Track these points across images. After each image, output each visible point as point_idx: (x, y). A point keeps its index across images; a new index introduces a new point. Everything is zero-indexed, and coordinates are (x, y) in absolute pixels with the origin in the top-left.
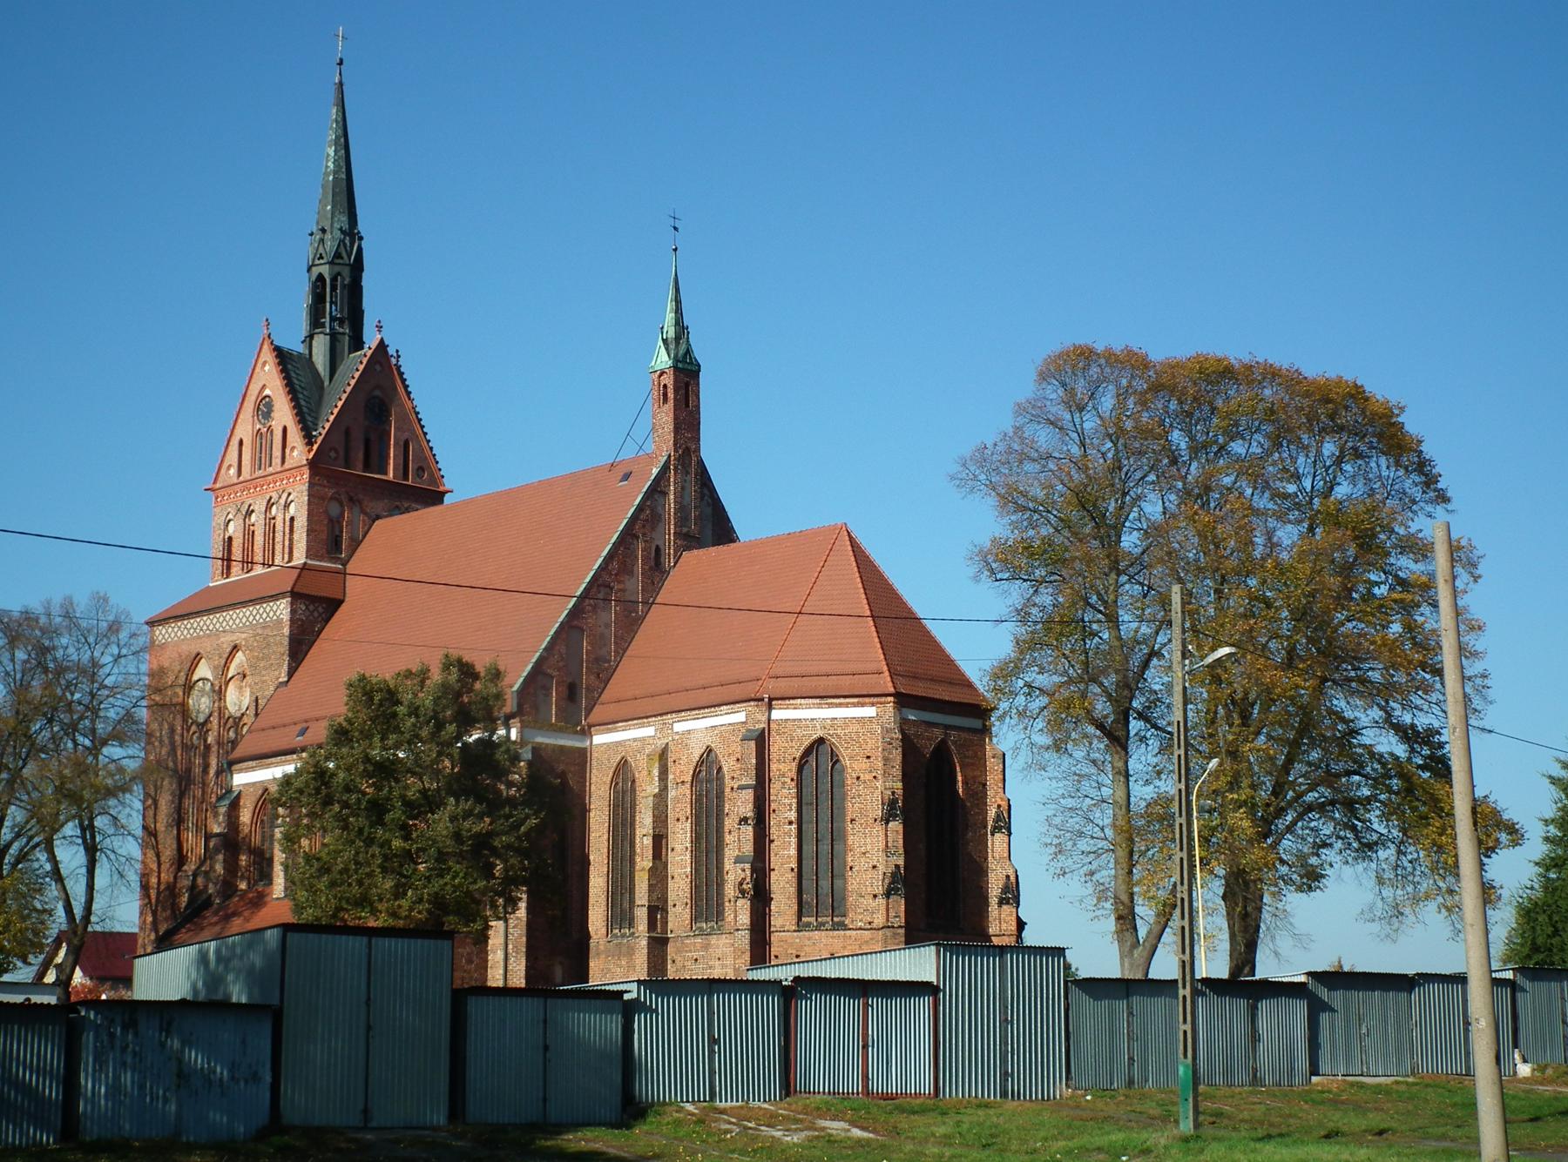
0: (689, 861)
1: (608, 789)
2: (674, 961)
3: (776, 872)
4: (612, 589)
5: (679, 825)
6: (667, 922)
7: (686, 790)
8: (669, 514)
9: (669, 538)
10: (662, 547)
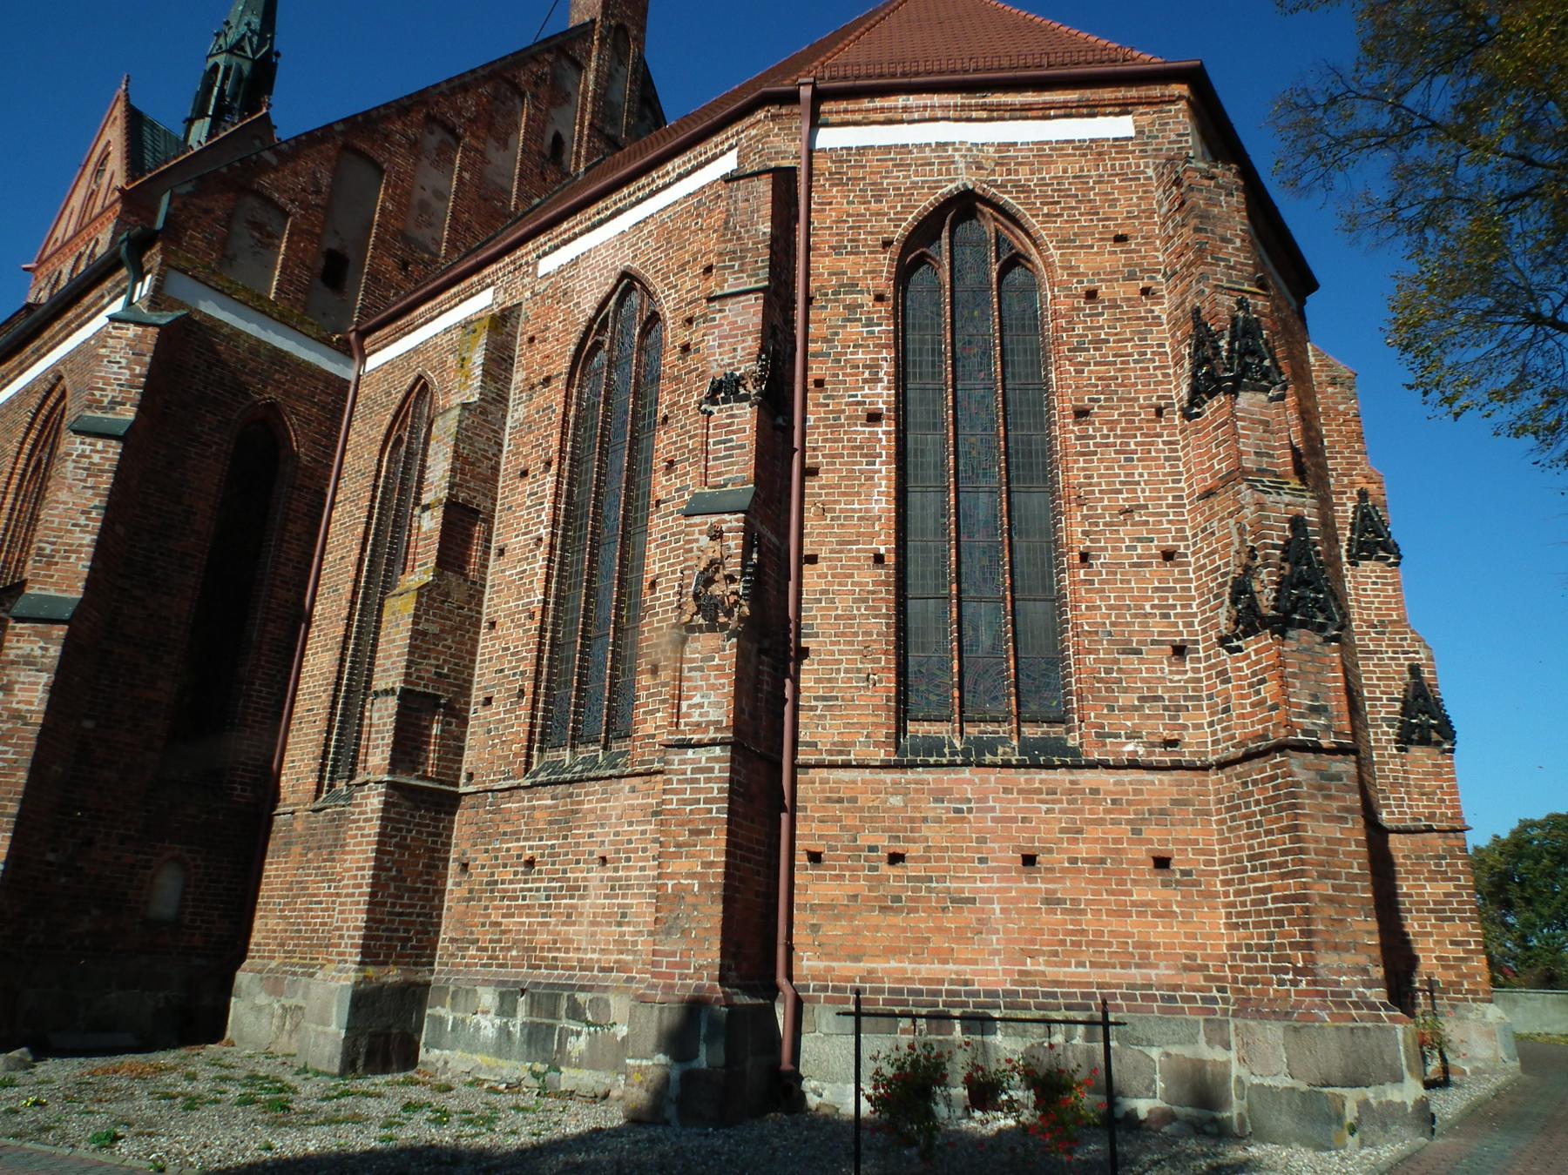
0: (541, 573)
1: (376, 453)
2: (465, 867)
3: (822, 566)
4: (458, 138)
5: (526, 486)
6: (460, 751)
7: (555, 396)
8: (584, 98)
9: (581, 132)
10: (566, 137)
